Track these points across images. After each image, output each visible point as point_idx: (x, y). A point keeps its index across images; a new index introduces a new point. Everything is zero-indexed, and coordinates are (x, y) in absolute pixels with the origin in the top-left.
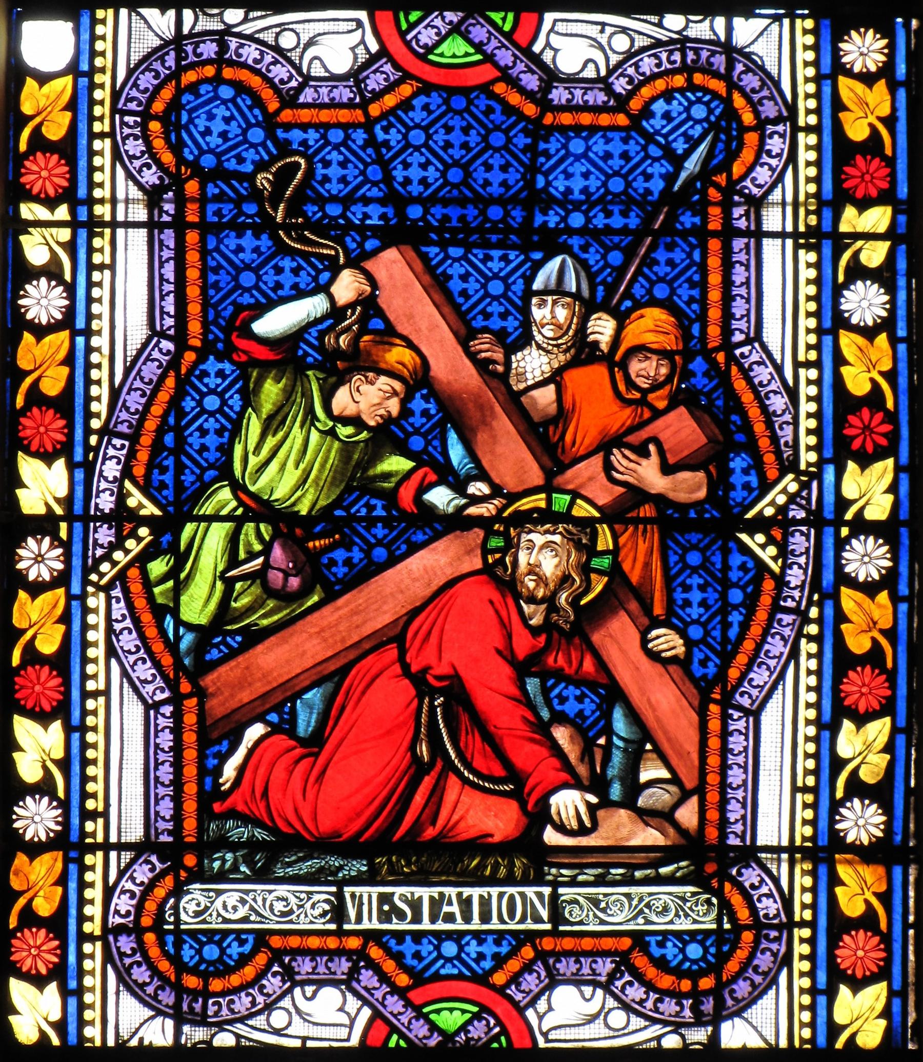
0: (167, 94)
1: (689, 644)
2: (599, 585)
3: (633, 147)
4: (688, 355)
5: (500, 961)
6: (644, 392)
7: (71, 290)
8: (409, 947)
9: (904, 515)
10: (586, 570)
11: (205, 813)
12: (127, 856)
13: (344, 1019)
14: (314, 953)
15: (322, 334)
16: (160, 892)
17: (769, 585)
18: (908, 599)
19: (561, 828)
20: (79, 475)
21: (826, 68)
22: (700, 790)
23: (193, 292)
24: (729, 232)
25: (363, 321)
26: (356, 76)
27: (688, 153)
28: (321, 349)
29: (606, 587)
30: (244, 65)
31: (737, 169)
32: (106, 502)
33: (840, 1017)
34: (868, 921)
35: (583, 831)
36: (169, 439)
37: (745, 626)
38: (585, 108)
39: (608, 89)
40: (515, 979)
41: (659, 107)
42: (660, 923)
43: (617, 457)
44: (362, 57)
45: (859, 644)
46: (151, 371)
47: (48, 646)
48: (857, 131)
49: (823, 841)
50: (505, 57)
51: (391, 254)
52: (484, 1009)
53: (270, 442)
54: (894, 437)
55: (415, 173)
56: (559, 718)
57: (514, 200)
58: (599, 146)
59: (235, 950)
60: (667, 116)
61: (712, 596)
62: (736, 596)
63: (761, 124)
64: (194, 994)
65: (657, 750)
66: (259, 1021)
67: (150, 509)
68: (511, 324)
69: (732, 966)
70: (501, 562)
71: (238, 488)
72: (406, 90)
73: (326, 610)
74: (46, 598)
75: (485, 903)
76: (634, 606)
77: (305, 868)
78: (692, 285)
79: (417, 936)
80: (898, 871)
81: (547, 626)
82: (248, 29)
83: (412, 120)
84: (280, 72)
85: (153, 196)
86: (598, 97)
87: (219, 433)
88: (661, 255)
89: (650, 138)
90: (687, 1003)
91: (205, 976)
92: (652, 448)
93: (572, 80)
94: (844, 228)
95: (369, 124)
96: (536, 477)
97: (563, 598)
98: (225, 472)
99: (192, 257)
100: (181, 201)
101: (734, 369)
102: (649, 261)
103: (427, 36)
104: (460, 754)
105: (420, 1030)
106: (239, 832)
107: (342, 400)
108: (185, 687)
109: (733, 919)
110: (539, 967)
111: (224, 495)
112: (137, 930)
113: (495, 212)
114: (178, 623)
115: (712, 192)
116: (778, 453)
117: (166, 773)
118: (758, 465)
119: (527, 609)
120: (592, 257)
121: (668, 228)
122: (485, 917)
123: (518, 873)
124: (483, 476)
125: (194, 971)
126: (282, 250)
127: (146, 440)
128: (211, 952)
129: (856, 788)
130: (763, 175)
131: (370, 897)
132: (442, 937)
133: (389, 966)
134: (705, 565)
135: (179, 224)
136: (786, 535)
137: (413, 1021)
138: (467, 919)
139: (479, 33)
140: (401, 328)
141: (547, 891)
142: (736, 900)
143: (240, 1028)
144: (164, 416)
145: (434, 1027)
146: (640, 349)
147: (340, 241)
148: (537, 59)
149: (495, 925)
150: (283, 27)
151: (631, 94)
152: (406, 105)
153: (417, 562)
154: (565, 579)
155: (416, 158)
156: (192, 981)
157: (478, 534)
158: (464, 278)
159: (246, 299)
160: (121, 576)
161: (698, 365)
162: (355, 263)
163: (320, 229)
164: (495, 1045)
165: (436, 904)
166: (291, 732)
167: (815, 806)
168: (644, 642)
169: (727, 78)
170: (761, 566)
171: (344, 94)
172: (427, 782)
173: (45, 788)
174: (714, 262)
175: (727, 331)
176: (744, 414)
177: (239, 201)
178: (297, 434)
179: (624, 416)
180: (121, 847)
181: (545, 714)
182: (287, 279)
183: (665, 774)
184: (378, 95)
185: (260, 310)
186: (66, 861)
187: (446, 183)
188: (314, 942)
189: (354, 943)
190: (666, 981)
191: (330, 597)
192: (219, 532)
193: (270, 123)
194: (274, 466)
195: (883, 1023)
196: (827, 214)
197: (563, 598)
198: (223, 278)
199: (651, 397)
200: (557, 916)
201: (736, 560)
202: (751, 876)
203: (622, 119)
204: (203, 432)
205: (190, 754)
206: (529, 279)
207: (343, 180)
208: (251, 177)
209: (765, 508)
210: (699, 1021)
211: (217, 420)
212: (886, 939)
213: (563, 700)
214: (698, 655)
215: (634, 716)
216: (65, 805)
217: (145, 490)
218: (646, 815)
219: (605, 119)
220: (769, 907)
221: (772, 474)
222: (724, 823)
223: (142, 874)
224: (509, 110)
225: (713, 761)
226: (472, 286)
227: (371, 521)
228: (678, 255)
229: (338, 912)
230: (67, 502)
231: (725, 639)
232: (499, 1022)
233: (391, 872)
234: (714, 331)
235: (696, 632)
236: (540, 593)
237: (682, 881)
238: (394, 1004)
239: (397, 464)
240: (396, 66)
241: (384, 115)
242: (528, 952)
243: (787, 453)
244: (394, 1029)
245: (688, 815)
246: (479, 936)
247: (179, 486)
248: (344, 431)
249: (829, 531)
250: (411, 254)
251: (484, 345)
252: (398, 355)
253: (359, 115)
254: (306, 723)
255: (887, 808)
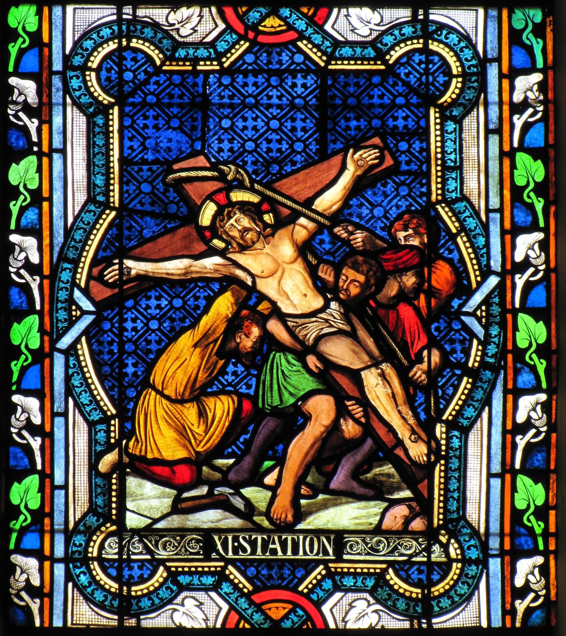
52: (296, 605)
83: (246, 135)
122: (295, 551)
131: (312, 550)
137: (254, 614)
138: (284, 551)
145: (267, 617)
149: (301, 556)
164: (305, 627)
211: (157, 335)
238: (243, 603)
244: (242, 617)
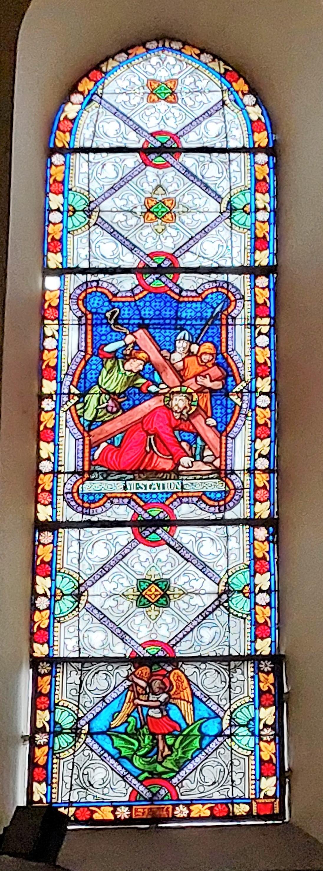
0: (83, 295)
1: (217, 422)
2: (194, 409)
3: (203, 305)
4: (217, 354)
5: (167, 499)
6: (206, 363)
7: (58, 341)
8: (143, 496)
9: (273, 390)
10: (190, 405)
11: (90, 464)
12: (70, 475)
13: (127, 513)
14: (118, 498)
15: (122, 351)
16: (78, 483)
17: (238, 408)
18: (275, 410)
19: (183, 466)
20: (59, 384)
21: (252, 287)
22: (220, 457)
23: (89, 341)
24: (227, 324)
25: (133, 347)
26: (132, 290)
27: (217, 307)
28: (122, 354)
29: (196, 409)
30: (103, 288)
31: (230, 310)
32: (66, 391)
33: (255, 140)
34: (264, 487)
35: (189, 467)
36: (82, 376)
37: (232, 418)
38: (191, 296)
39: (197, 292)
40: (172, 503)
41: (210, 296)
42: (210, 489)
43: (199, 378)
44: (134, 286)
45: (261, 422)
46: (78, 360)
47: (50, 425)
48: (260, 301)
49: (252, 468)
50: (170, 285)
51: (141, 331)
53: (109, 376)
54: (270, 373)
55: (147, 312)
56: (183, 440)
57: (173, 318)
58: (194, 305)
59: (98, 497)
60: (212, 298)
61: (223, 411)
62: (229, 411)
63: (236, 300)
64: (87, 508)
65: (209, 448)
66: (104, 514)
67: (77, 392)
68: (172, 348)
69: (228, 499)
70: (168, 404)
71: (100, 387)
72: (145, 293)
73: (123, 415)
74: (49, 414)
75: (163, 485)
76: (203, 413)
77: (117, 477)
78: (218, 337)
79: (146, 493)
80: (272, 475)
81: (180, 418)
82: (104, 279)
84: (112, 289)
85: (80, 318)
86: (194, 294)
87: (96, 374)
88: (210, 331)
89: (208, 303)
90: (217, 508)
91: (90, 504)
92: (208, 376)
93: (187, 290)
94: (257, 323)
95: (135, 301)
96: (179, 384)
97: (184, 412)
98: (97, 383)
99: (89, 333)
100: (87, 319)
101: (229, 357)
102: (207, 332)
103: (150, 280)
104: (157, 449)
105: (146, 516)
106: (98, 468)
107: (128, 366)
108: (86, 434)
109: (229, 487)
110: (178, 500)
111: (97, 388)
112: (72, 493)
113: (168, 321)
114: (84, 419)
115: (223, 316)
116: (240, 377)
117: (80, 455)
118: (235, 379)
119: (175, 414)
120: (193, 331)
121: (212, 324)
122: (164, 488)
123: (172, 477)
124: (163, 383)
125: (87, 502)
126: (112, 330)
127: (77, 376)
128: (91, 498)
129: (260, 456)
130: (236, 311)
132: (153, 493)
133: (138, 500)
134: (221, 404)
135: (86, 324)
136: (242, 396)
139: (164, 279)
140: (143, 349)
141: (180, 482)
142: (230, 483)
143: (99, 516)
144: (81, 371)
145: (150, 515)
146: (205, 353)
147: (127, 328)
148: (178, 285)
150: (113, 279)
151: (202, 293)
152: (145, 296)
153: (146, 404)
154: (185, 408)
155: (148, 309)
156: (87, 505)
157: (163, 397)
158: (160, 337)
159: (103, 342)
160: (69, 409)
161: (220, 356)
162: (132, 333)
163: (122, 325)
165: (151, 486)
166: (113, 445)
167: (250, 460)
168: (205, 422)
169: (227, 289)
170: (236, 404)
171: (129, 294)
172: (149, 456)
173: (49, 459)
174: (224, 332)
175: (227, 348)
176: (231, 367)
177: (102, 319)
178: (116, 374)
179: (201, 369)
180: (68, 473)
181: (180, 440)
182: (114, 338)
183: (211, 453)
184: (137, 294)
185: (106, 345)
186: (54, 476)
187: (155, 315)
188: (119, 495)
189: (129, 495)
190: (211, 503)
191: (124, 412)
192: (96, 397)
193: (110, 301)
194: (110, 381)
195: (269, 511)
196: (253, 320)
197: (184, 412)
198: (97, 338)
199: (208, 364)
200: (182, 487)
201: (229, 402)
202: (233, 477)
203: (200, 299)
204: (91, 374)
205: (87, 451)
206: (176, 336)
207: (129, 314)
208: (105, 314)
209: (237, 389)
210: (220, 512)
212: (269, 492)
213: (184, 436)
214: (220, 425)
215: (202, 440)
216: (53, 463)
217: (76, 387)
218: (206, 463)
219: (196, 299)
220: (238, 484)
221: (238, 382)
222: (226, 465)
223: (74, 479)
224: (171, 297)
225: (223, 450)
226: (162, 338)
227: (135, 394)
228: (215, 331)
229: (125, 488)
230: (56, 392)
231: (226, 422)
232: (167, 513)
233: (140, 477)
234: (224, 349)
235: (219, 420)
236: (179, 411)
237: (216, 478)
238: (139, 510)
239: (141, 381)
240: (143, 288)
241: (140, 299)
242: (175, 496)
243: (243, 377)
245: (217, 463)
246: (162, 493)
247: (85, 387)
248: (128, 373)
249: (253, 394)
250: (146, 331)
251: (164, 353)
252: (142, 355)
253: (133, 299)
254: (117, 443)
255: (269, 460)
